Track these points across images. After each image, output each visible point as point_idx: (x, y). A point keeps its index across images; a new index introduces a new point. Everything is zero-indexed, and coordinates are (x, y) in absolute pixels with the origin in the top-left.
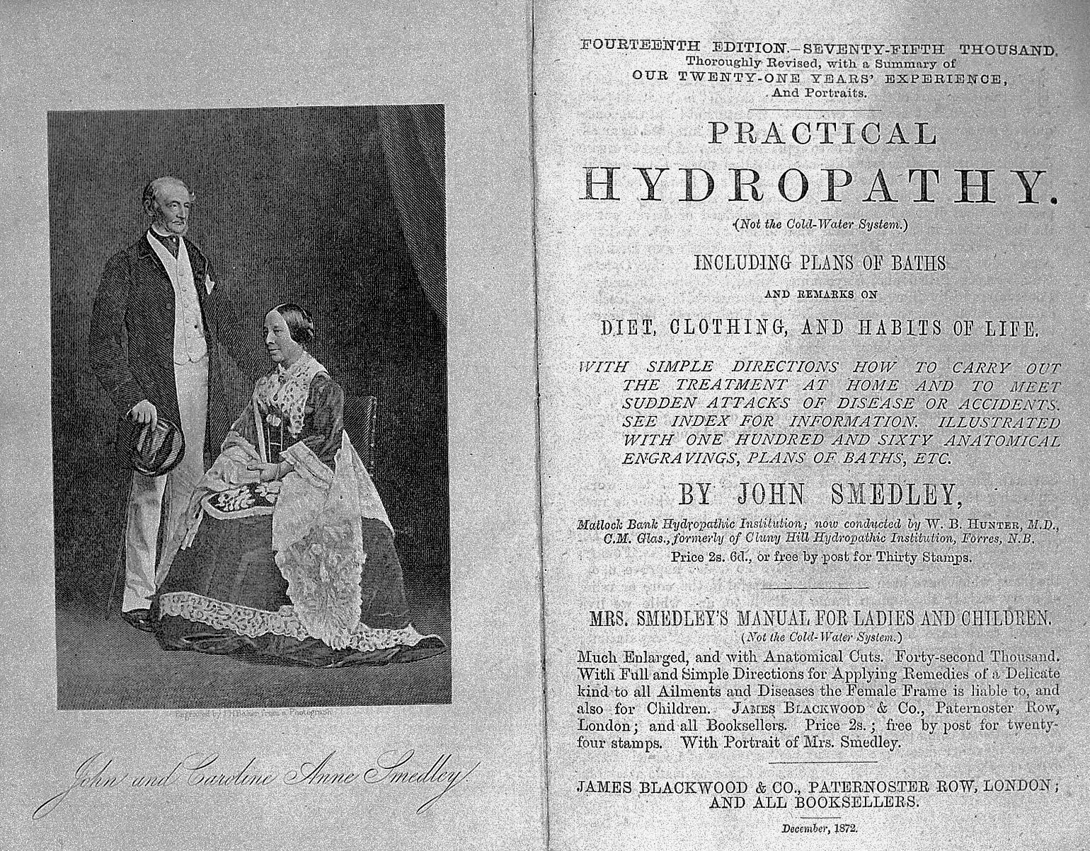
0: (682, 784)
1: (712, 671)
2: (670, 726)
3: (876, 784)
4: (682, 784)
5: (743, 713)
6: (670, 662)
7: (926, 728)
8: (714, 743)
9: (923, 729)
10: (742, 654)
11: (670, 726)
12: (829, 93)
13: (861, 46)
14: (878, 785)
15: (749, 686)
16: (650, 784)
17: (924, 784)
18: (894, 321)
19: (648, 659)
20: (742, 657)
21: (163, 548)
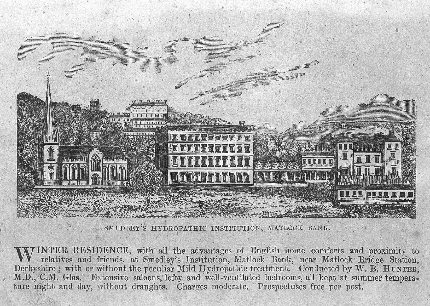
0: (121, 248)
1: (390, 249)
2: (361, 251)
3: (116, 249)
4: (121, 248)
5: (383, 253)
6: (200, 289)
7: (31, 270)
8: (277, 251)
9: (266, 279)
10: (145, 249)
11: (361, 251)
12: (338, 250)
13: (48, 248)
14: (118, 249)
15: (194, 266)
16: (79, 248)
17: (64, 249)
18: (75, 247)
19: (51, 260)
20: (398, 250)
21: (88, 200)
